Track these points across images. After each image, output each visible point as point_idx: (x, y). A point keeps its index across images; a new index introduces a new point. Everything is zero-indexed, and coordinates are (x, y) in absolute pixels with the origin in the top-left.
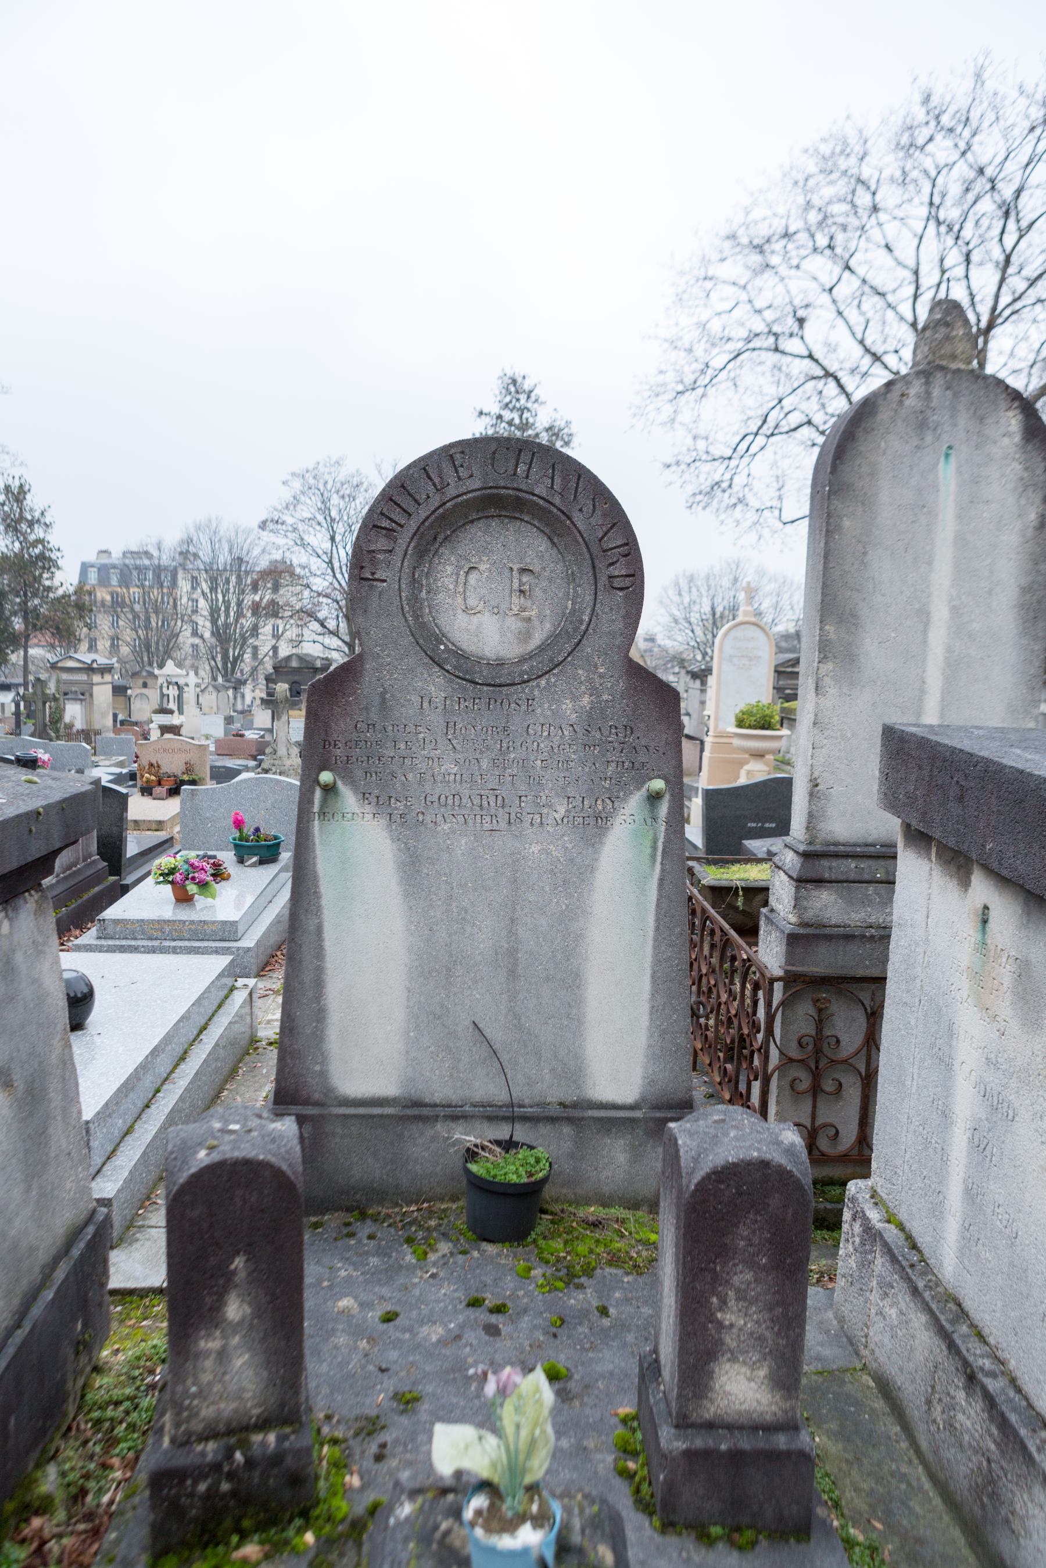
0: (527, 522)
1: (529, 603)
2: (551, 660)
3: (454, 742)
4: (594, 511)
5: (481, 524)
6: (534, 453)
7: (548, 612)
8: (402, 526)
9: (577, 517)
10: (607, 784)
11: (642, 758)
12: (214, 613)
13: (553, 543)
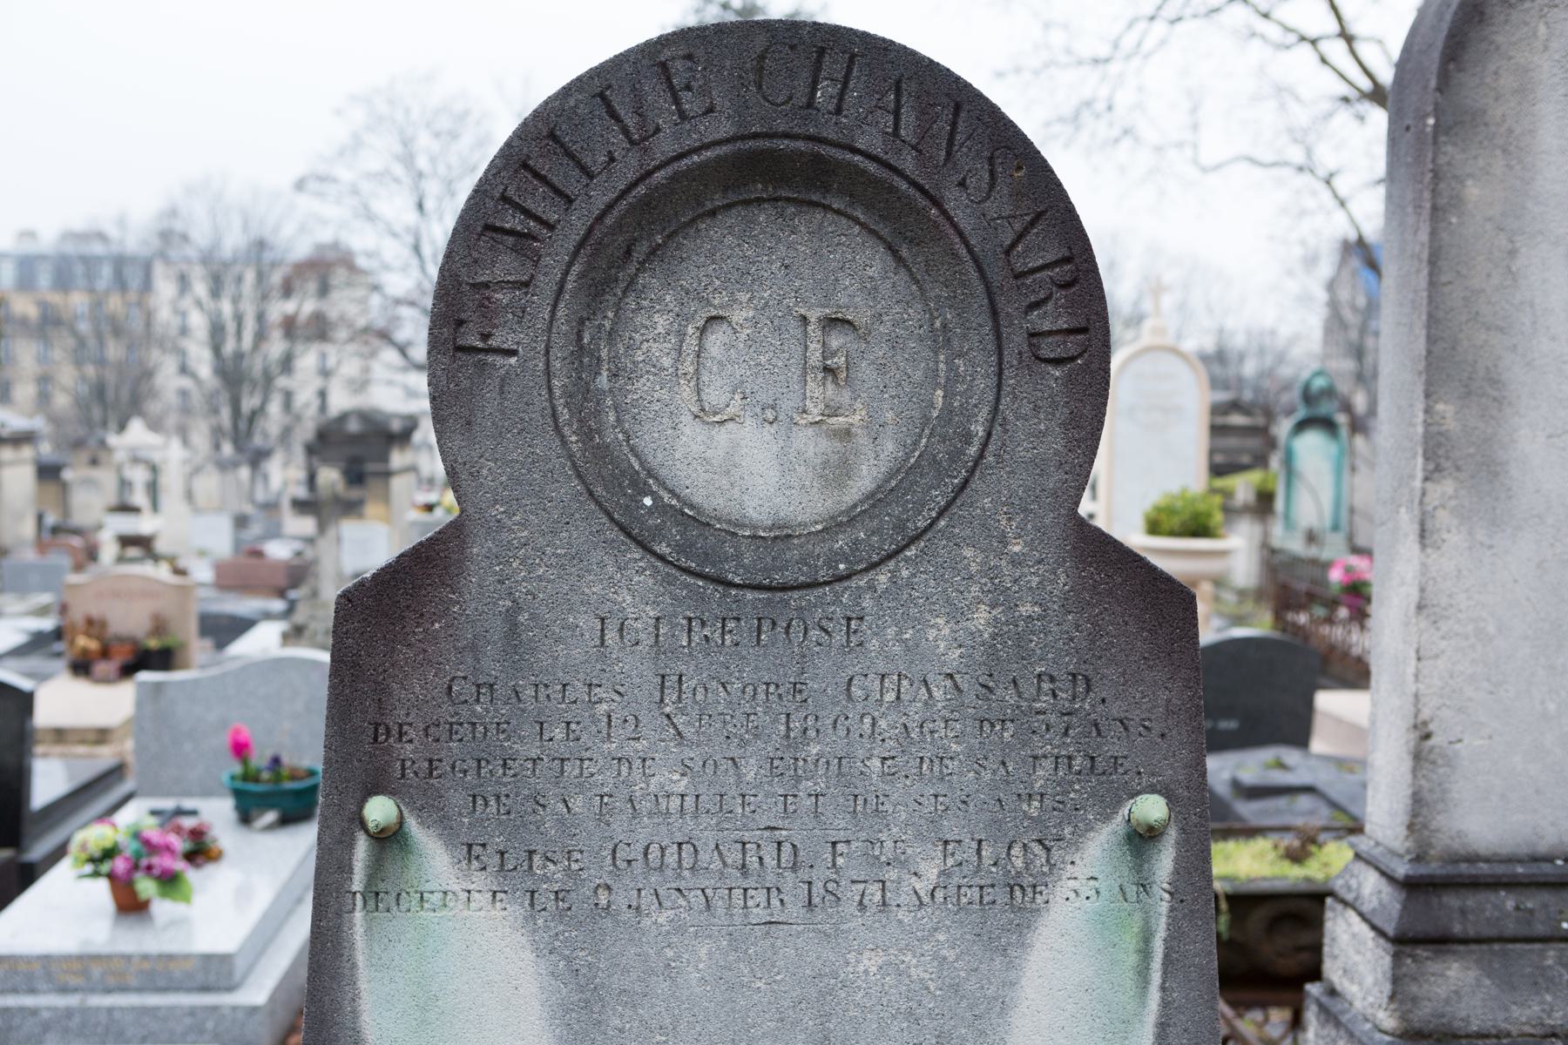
0: (838, 212)
1: (846, 396)
2: (900, 526)
3: (679, 720)
4: (992, 186)
5: (731, 219)
6: (852, 57)
7: (890, 415)
8: (551, 227)
9: (956, 202)
10: (1034, 808)
11: (1113, 746)
12: (217, 332)
13: (899, 260)
